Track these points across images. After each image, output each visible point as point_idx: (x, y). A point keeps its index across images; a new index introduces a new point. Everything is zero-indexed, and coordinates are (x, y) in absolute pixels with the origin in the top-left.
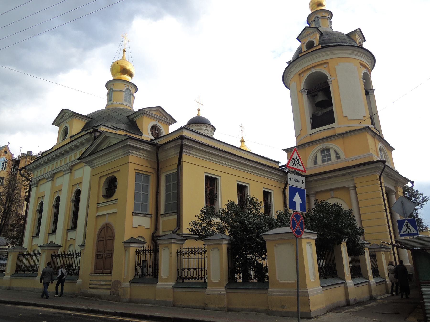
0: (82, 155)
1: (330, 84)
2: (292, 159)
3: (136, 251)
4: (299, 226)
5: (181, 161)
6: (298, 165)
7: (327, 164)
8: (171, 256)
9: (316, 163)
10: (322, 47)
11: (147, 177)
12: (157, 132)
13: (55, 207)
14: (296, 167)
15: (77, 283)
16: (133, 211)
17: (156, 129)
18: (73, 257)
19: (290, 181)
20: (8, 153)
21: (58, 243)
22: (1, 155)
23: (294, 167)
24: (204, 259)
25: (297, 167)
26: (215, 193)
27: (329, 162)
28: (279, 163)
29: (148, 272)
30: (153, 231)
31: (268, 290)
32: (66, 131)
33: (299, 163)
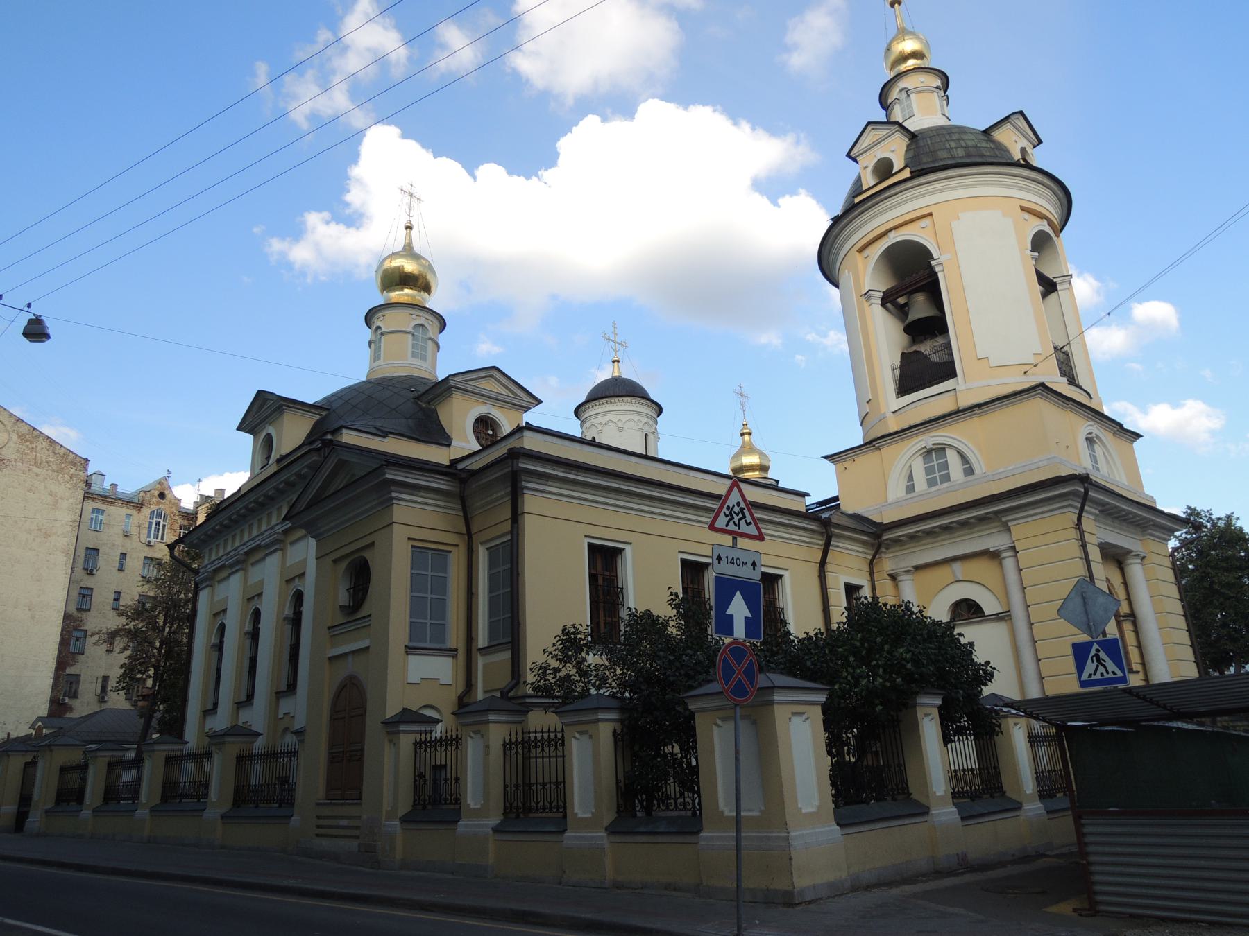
0: (291, 507)
1: (940, 272)
2: (725, 509)
3: (415, 744)
4: (741, 675)
5: (519, 513)
6: (741, 522)
7: (939, 490)
8: (487, 754)
9: (911, 489)
10: (914, 174)
11: (441, 555)
12: (490, 432)
13: (250, 636)
14: (736, 529)
15: (458, 829)
16: (407, 644)
17: (487, 423)
18: (289, 759)
19: (719, 563)
20: (168, 496)
21: (257, 726)
22: (151, 503)
23: (732, 527)
24: (562, 759)
25: (739, 528)
26: (618, 588)
27: (946, 485)
28: (803, 495)
29: (453, 792)
30: (460, 690)
31: (701, 834)
32: (268, 443)
33: (744, 516)
